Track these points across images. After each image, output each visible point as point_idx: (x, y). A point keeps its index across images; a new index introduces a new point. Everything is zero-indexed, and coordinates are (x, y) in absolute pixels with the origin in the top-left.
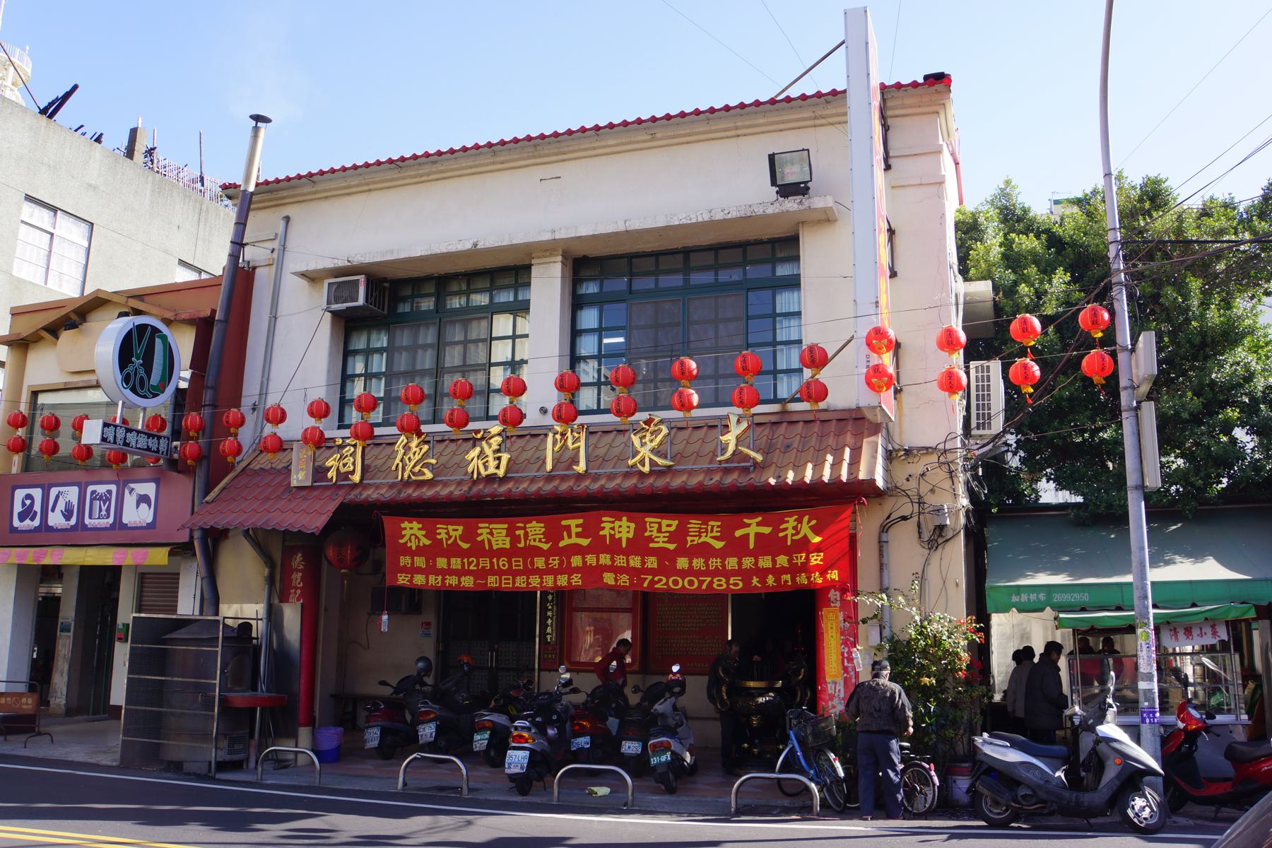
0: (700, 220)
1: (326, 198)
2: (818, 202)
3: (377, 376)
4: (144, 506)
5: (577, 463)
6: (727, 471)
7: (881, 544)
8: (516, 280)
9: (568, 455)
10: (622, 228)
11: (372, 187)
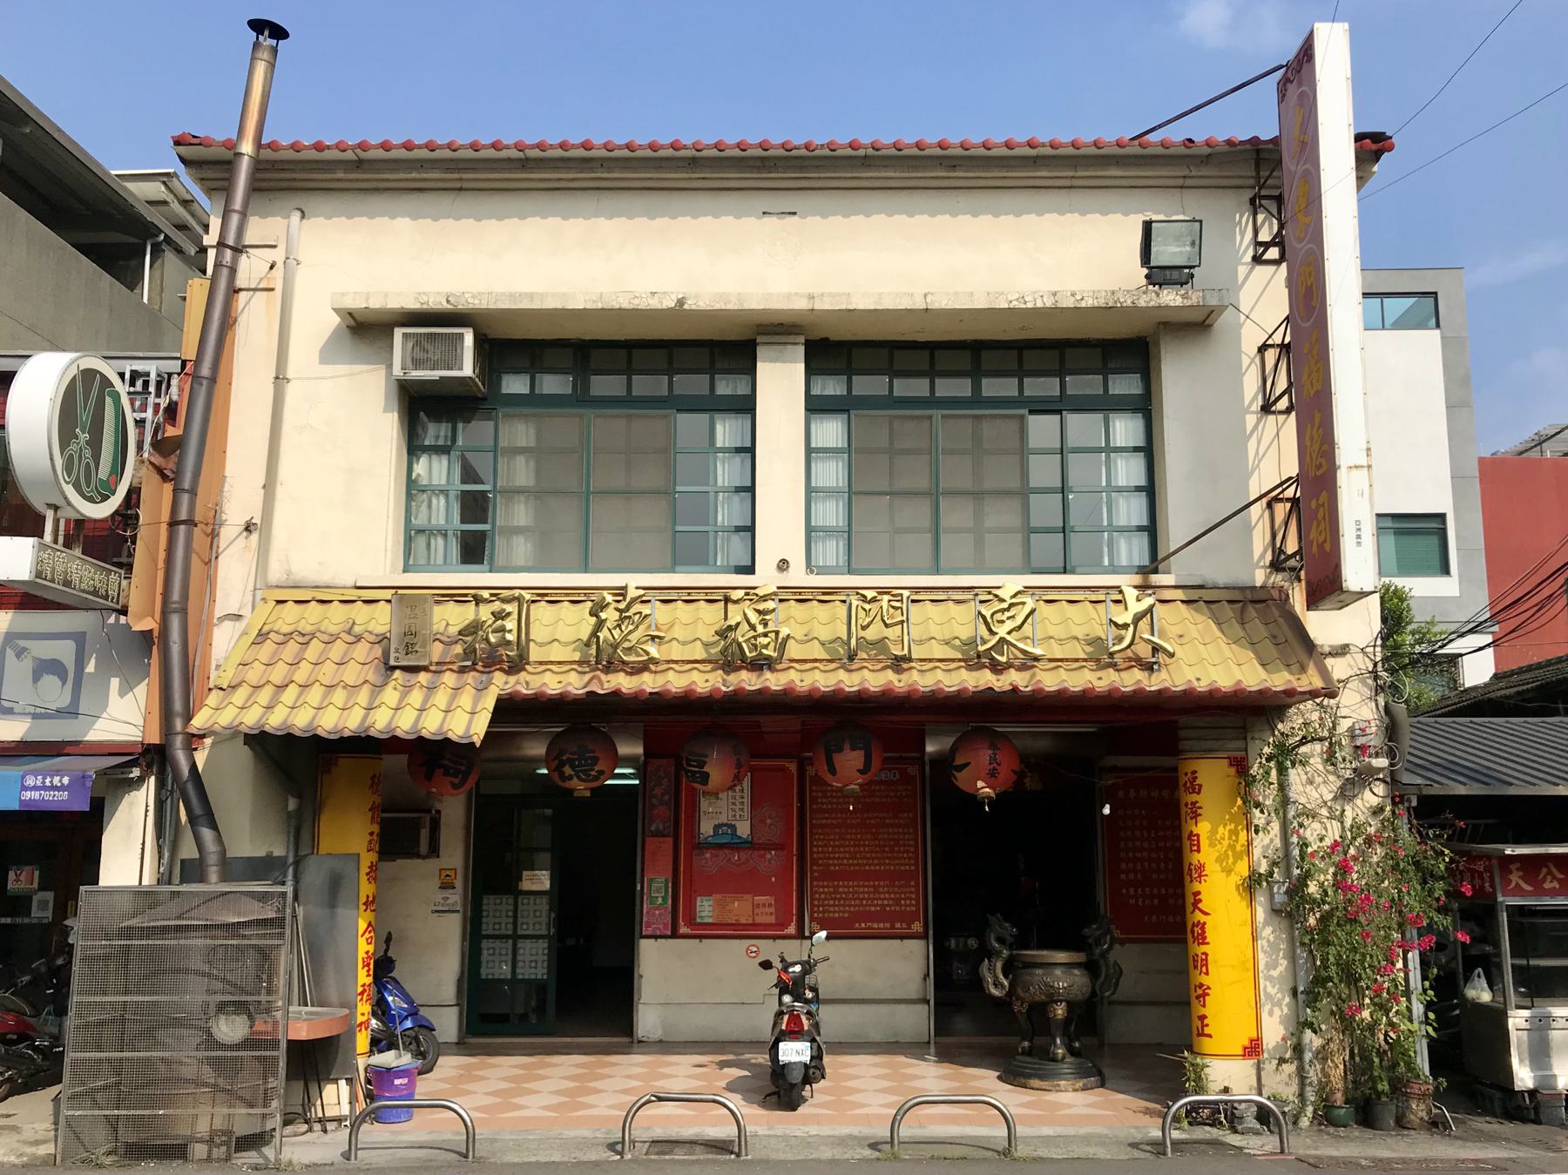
0: (1039, 304)
4: (50, 681)
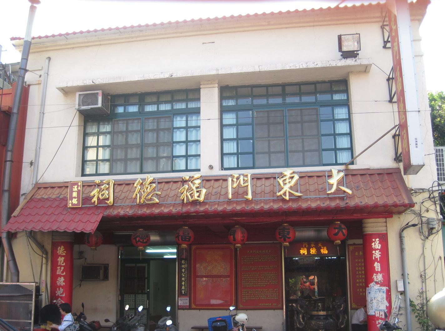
0: (301, 67)
1: (73, 48)
2: (362, 60)
3: (152, 145)
5: (247, 194)
6: (331, 199)
7: (401, 238)
8: (158, 99)
9: (241, 191)
10: (257, 69)
11: (102, 43)
